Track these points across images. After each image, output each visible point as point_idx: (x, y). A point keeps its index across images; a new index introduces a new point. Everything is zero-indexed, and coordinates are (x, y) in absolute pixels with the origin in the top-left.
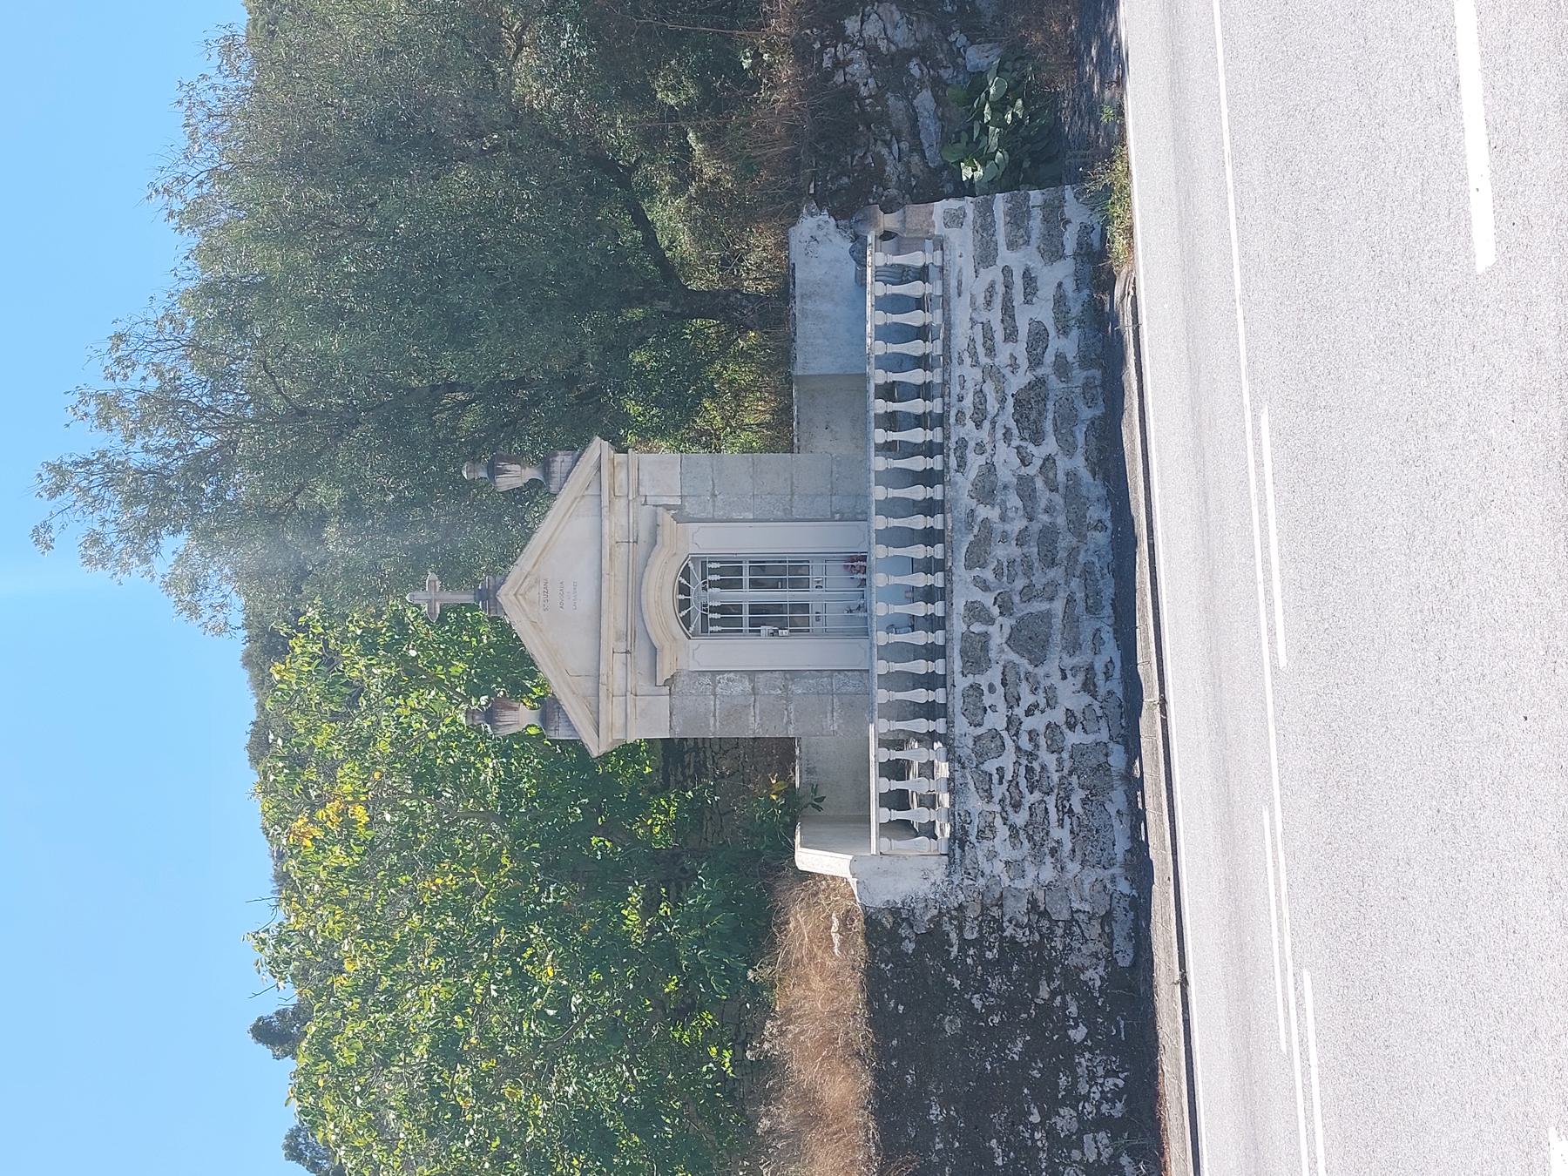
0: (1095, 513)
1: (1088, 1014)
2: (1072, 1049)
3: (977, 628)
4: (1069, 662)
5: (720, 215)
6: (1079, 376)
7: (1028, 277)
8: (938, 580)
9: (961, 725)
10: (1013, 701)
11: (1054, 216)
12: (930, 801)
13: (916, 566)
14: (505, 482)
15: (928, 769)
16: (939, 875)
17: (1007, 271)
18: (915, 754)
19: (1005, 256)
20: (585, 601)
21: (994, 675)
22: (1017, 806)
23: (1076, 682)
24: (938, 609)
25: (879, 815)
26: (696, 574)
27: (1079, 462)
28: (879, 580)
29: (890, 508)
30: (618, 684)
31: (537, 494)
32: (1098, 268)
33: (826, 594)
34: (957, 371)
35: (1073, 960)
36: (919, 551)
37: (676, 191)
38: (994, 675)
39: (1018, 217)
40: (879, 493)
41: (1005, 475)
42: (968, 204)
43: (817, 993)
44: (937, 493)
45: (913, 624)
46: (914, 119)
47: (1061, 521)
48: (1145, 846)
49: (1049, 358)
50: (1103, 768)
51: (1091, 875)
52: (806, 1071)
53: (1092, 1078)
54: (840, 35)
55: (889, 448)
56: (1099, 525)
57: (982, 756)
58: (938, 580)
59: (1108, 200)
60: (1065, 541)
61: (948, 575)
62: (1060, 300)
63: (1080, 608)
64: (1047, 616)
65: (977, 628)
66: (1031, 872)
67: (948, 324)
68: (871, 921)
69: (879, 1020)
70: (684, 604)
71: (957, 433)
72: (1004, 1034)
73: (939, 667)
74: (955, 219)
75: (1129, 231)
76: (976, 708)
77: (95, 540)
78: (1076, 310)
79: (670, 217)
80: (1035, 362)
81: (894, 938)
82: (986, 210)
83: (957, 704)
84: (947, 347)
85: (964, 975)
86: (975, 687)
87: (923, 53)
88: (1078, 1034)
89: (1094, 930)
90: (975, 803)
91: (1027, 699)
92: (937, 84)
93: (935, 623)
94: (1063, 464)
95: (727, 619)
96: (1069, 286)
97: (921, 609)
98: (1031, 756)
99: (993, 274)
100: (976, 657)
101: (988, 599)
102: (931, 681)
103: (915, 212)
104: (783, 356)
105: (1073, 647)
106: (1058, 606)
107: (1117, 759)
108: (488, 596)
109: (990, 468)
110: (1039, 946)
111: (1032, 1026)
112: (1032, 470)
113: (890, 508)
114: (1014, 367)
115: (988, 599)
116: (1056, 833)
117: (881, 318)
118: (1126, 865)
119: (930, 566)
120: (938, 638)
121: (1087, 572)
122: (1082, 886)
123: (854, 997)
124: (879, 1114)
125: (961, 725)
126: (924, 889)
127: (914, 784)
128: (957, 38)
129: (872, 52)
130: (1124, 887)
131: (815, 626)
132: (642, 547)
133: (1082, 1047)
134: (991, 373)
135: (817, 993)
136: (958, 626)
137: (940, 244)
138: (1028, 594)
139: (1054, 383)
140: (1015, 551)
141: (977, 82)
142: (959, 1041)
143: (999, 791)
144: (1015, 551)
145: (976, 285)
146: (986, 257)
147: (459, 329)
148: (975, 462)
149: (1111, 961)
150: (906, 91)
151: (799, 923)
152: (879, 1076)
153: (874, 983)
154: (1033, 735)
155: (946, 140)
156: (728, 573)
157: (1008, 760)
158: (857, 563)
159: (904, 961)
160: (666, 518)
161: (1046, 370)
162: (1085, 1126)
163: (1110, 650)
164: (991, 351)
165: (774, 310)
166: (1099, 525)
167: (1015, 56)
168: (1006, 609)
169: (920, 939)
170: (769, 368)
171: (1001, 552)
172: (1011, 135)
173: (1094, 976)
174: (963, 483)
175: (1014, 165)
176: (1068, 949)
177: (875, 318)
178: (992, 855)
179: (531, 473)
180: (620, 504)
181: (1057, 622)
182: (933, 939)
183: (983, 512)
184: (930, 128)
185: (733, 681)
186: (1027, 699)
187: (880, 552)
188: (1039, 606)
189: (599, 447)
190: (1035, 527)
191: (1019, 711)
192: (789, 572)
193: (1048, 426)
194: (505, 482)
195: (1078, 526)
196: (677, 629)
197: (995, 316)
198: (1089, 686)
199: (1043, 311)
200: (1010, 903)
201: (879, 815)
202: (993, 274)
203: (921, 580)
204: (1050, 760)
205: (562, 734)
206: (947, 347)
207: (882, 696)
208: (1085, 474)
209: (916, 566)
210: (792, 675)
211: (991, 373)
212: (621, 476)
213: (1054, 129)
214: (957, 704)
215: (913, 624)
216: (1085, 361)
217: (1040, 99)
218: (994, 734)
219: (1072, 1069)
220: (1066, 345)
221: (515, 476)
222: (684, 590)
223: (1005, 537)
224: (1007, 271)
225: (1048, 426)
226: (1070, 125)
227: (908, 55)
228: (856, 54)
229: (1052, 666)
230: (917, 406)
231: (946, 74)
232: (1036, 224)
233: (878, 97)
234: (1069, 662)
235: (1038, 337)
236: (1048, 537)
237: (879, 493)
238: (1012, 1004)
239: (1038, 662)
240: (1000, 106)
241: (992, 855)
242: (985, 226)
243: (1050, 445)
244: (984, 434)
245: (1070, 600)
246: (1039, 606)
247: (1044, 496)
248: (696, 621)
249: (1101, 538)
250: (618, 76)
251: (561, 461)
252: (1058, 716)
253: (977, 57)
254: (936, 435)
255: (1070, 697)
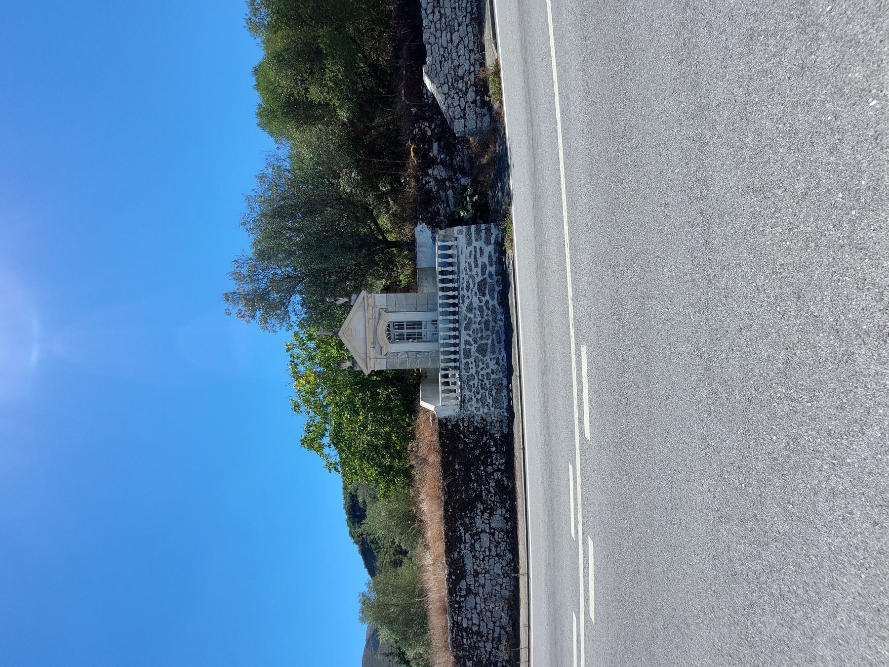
0: (499, 316)
1: (496, 445)
2: (492, 453)
3: (468, 347)
4: (492, 356)
5: (398, 220)
6: (495, 278)
7: (481, 249)
8: (457, 333)
9: (463, 372)
10: (477, 366)
11: (488, 232)
12: (455, 384)
13: (451, 321)
14: (338, 303)
15: (454, 376)
16: (458, 410)
17: (475, 247)
18: (450, 373)
19: (474, 243)
20: (362, 335)
21: (472, 359)
22: (478, 393)
23: (494, 362)
24: (457, 341)
25: (441, 388)
26: (392, 326)
27: (495, 302)
28: (441, 326)
29: (443, 305)
30: (372, 356)
31: (347, 308)
32: (501, 249)
33: (427, 331)
34: (461, 276)
35: (492, 432)
36: (452, 317)
37: (386, 213)
38: (472, 359)
39: (478, 232)
40: (440, 301)
41: (475, 305)
42: (464, 228)
43: (426, 438)
44: (456, 309)
45: (450, 337)
46: (447, 198)
47: (490, 318)
48: (512, 407)
49: (487, 273)
50: (501, 384)
51: (497, 411)
52: (423, 451)
53: (497, 460)
54: (427, 174)
55: (443, 289)
56: (501, 320)
57: (469, 380)
58: (457, 333)
59: (505, 232)
60: (492, 324)
61: (460, 332)
62: (490, 256)
63: (495, 343)
64: (486, 344)
65: (468, 347)
66: (482, 410)
67: (459, 262)
68: (440, 421)
69: (443, 445)
70: (389, 334)
71: (462, 293)
72: (474, 449)
73: (457, 357)
74: (460, 232)
75: (512, 240)
76: (467, 369)
77: (240, 312)
78: (494, 259)
79: (384, 221)
80: (483, 274)
81: (446, 425)
82: (469, 230)
83: (462, 367)
84: (458, 269)
85: (464, 434)
86: (467, 362)
87: (450, 179)
88: (493, 449)
89: (498, 424)
90: (467, 393)
91: (481, 366)
92: (453, 188)
93: (455, 345)
94: (491, 303)
95: (401, 338)
96: (492, 252)
97: (452, 333)
98: (482, 381)
99: (471, 248)
100: (467, 354)
101: (471, 339)
102: (455, 360)
103: (449, 230)
104: (414, 260)
105: (493, 352)
106: (490, 342)
107: (505, 382)
108: (336, 333)
109: (471, 303)
110: (483, 428)
111: (482, 447)
112: (483, 304)
113: (443, 305)
114: (477, 275)
115: (471, 339)
116: (488, 400)
117: (440, 260)
118: (507, 409)
119: (454, 329)
120: (457, 349)
121: (498, 332)
122: (494, 413)
123: (435, 438)
124: (442, 466)
125: (463, 372)
126: (454, 413)
127: (451, 380)
128: (459, 175)
129: (436, 179)
130: (506, 414)
131: (424, 339)
132: (377, 319)
133: (494, 452)
134: (471, 276)
135: (426, 438)
136: (463, 346)
137: (456, 239)
138: (481, 338)
139: (489, 280)
140: (478, 326)
141: (465, 188)
142: (463, 450)
143: (473, 390)
144: (478, 326)
145: (466, 251)
146: (469, 243)
147: (327, 258)
148: (467, 301)
149: (502, 432)
150: (445, 190)
151: (422, 417)
152: (443, 458)
153: (441, 436)
154: (482, 375)
155: (457, 204)
156: (400, 325)
157: (476, 382)
158: (434, 322)
159: (449, 432)
160: (383, 312)
161: (486, 276)
162: (494, 471)
163: (503, 354)
164: (471, 270)
165: (411, 245)
166: (501, 320)
167: (475, 182)
168: (475, 342)
169: (453, 426)
170: (410, 260)
171: (474, 326)
172: (474, 205)
173: (498, 436)
174: (463, 308)
175: (475, 214)
176: (491, 429)
177: (438, 260)
178: (472, 406)
179: (346, 300)
180: (370, 308)
181: (489, 346)
182: (456, 426)
183: (469, 315)
184: (452, 201)
185: (403, 355)
186: (481, 366)
187: (441, 318)
188: (484, 341)
189: (364, 293)
190: (483, 320)
191: (479, 369)
192: (419, 325)
193: (487, 292)
194: (338, 303)
195: (495, 320)
196: (387, 341)
197: (472, 260)
198: (497, 363)
199: (485, 259)
200: (476, 418)
201: (441, 388)
202: (471, 248)
203: (452, 326)
204: (487, 382)
205: (358, 369)
206: (458, 269)
207: (442, 357)
208: (497, 306)
209: (451, 321)
210: (418, 352)
211: (471, 276)
212: (370, 300)
213: (487, 204)
214: (462, 367)
215: (450, 337)
216: (497, 274)
217: (483, 195)
218: (472, 375)
219: (491, 457)
220: (492, 269)
221: (341, 301)
222: (388, 330)
223: (475, 322)
224: (475, 247)
225: (487, 292)
226: (492, 205)
227: (445, 180)
228: (431, 180)
229: (488, 357)
230: (451, 285)
231: (456, 185)
232: (483, 234)
233: (438, 192)
234: (492, 356)
235: (484, 267)
236: (487, 322)
237: (440, 301)
238: (477, 442)
239: (484, 356)
240: (471, 197)
241: (472, 406)
242: (469, 234)
243: (487, 297)
244: (469, 294)
245: (493, 340)
246: (484, 341)
247: (486, 311)
248: (392, 338)
249: (501, 323)
250: (369, 182)
251: (354, 297)
252: (489, 371)
253: (464, 181)
254: (456, 293)
255: (493, 365)
